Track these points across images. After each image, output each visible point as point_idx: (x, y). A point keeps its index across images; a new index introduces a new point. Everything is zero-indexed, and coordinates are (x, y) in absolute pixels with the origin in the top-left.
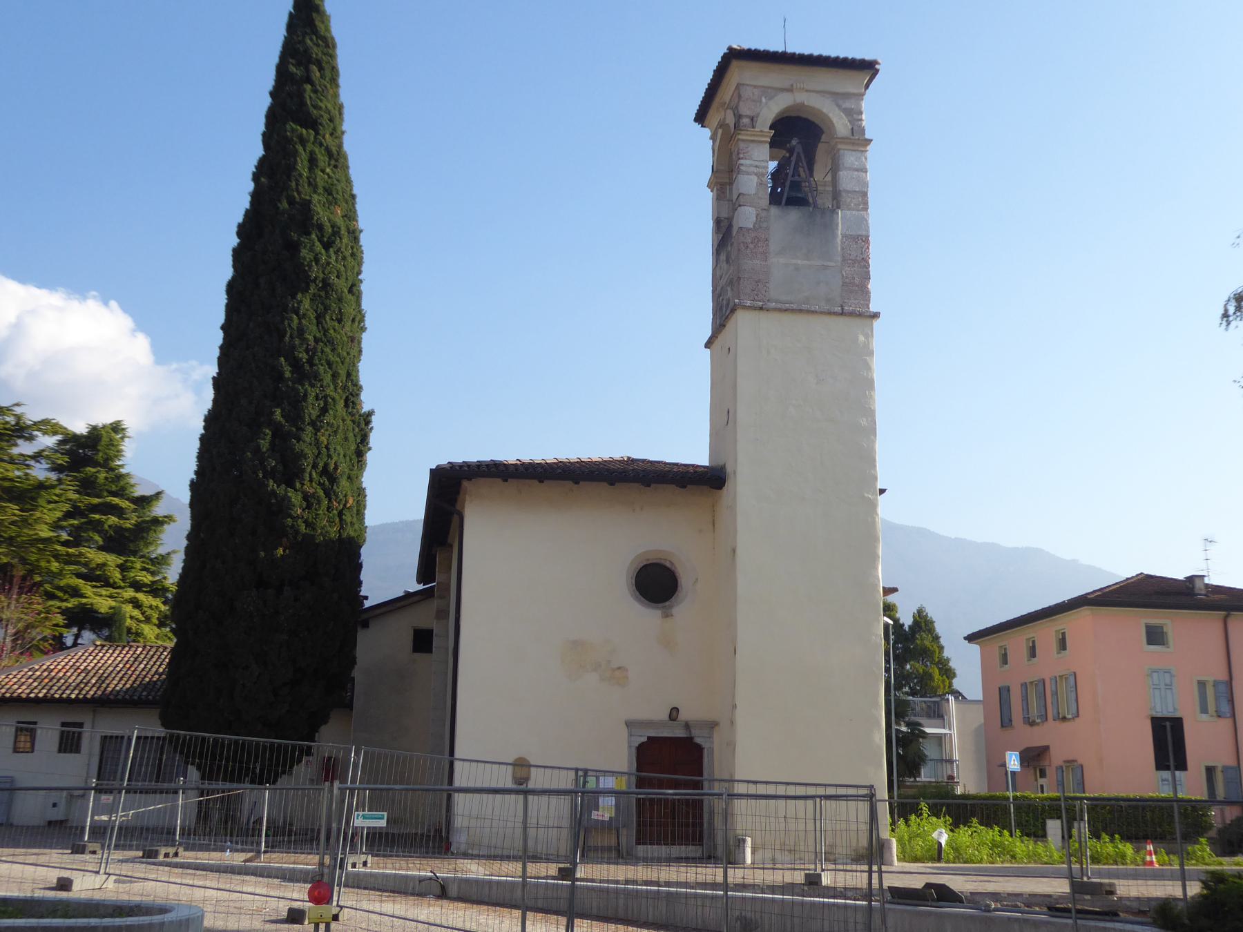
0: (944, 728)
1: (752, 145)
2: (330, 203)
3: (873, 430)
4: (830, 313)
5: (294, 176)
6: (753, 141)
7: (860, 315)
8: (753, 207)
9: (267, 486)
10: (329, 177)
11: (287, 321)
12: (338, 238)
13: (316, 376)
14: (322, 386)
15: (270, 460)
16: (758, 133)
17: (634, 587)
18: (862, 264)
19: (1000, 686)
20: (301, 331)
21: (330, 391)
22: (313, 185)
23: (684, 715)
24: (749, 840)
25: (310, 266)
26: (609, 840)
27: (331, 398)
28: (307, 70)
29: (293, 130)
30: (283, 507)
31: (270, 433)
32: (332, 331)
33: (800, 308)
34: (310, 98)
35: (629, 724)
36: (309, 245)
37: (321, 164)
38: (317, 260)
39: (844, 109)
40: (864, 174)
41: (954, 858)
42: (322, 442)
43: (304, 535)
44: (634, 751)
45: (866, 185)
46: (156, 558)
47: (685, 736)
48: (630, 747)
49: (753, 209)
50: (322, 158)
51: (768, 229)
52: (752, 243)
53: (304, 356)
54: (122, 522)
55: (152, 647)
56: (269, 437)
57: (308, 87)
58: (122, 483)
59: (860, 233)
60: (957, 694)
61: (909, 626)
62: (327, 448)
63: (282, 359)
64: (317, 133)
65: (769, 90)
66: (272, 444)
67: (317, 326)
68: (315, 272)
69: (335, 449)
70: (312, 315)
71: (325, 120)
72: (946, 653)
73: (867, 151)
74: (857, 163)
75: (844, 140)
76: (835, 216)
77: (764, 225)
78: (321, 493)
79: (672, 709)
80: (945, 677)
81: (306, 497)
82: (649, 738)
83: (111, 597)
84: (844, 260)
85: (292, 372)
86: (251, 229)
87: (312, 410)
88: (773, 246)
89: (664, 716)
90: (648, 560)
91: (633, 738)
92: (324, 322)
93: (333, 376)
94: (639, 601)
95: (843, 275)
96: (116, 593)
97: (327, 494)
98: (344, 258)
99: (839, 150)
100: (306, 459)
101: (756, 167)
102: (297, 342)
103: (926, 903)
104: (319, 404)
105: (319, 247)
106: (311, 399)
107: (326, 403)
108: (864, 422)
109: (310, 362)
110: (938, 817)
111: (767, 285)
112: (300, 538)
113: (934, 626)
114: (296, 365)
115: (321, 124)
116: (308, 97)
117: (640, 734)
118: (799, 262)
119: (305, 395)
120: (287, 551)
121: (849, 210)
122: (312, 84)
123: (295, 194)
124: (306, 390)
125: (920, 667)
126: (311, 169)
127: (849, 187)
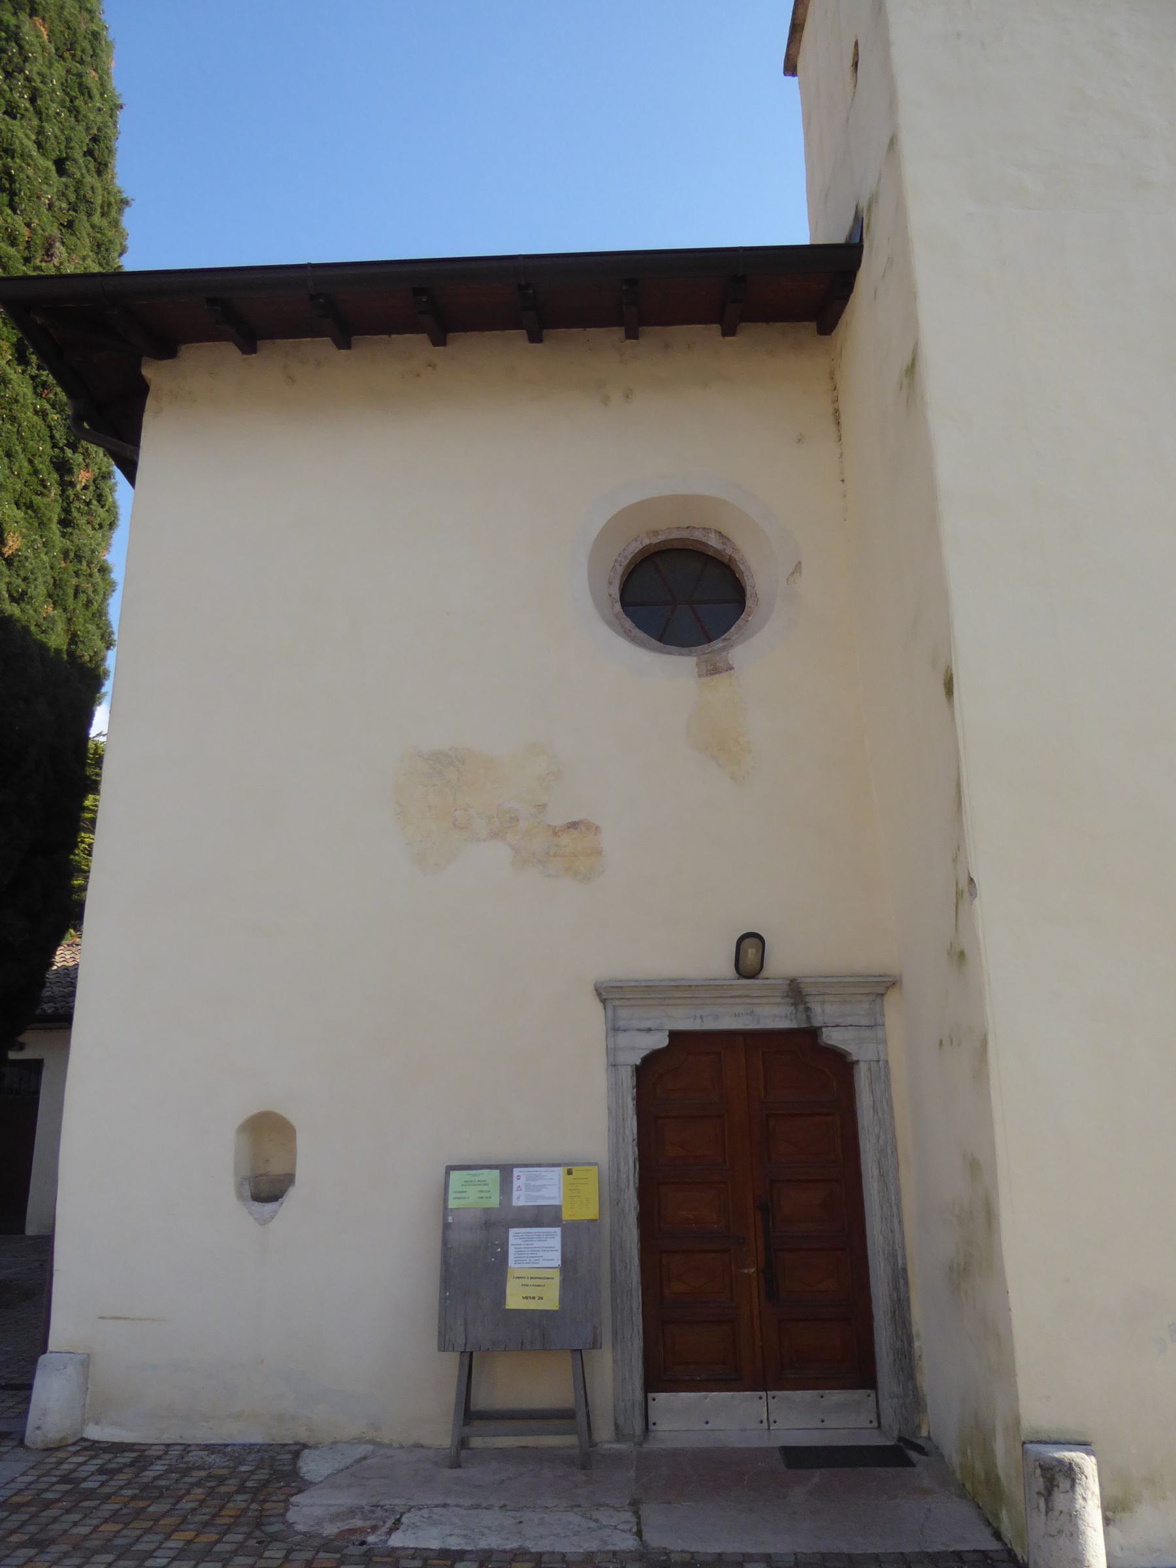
12: (13, 44)
44: (627, 1079)
47: (794, 1025)
48: (614, 1066)
89: (721, 964)
91: (623, 1039)
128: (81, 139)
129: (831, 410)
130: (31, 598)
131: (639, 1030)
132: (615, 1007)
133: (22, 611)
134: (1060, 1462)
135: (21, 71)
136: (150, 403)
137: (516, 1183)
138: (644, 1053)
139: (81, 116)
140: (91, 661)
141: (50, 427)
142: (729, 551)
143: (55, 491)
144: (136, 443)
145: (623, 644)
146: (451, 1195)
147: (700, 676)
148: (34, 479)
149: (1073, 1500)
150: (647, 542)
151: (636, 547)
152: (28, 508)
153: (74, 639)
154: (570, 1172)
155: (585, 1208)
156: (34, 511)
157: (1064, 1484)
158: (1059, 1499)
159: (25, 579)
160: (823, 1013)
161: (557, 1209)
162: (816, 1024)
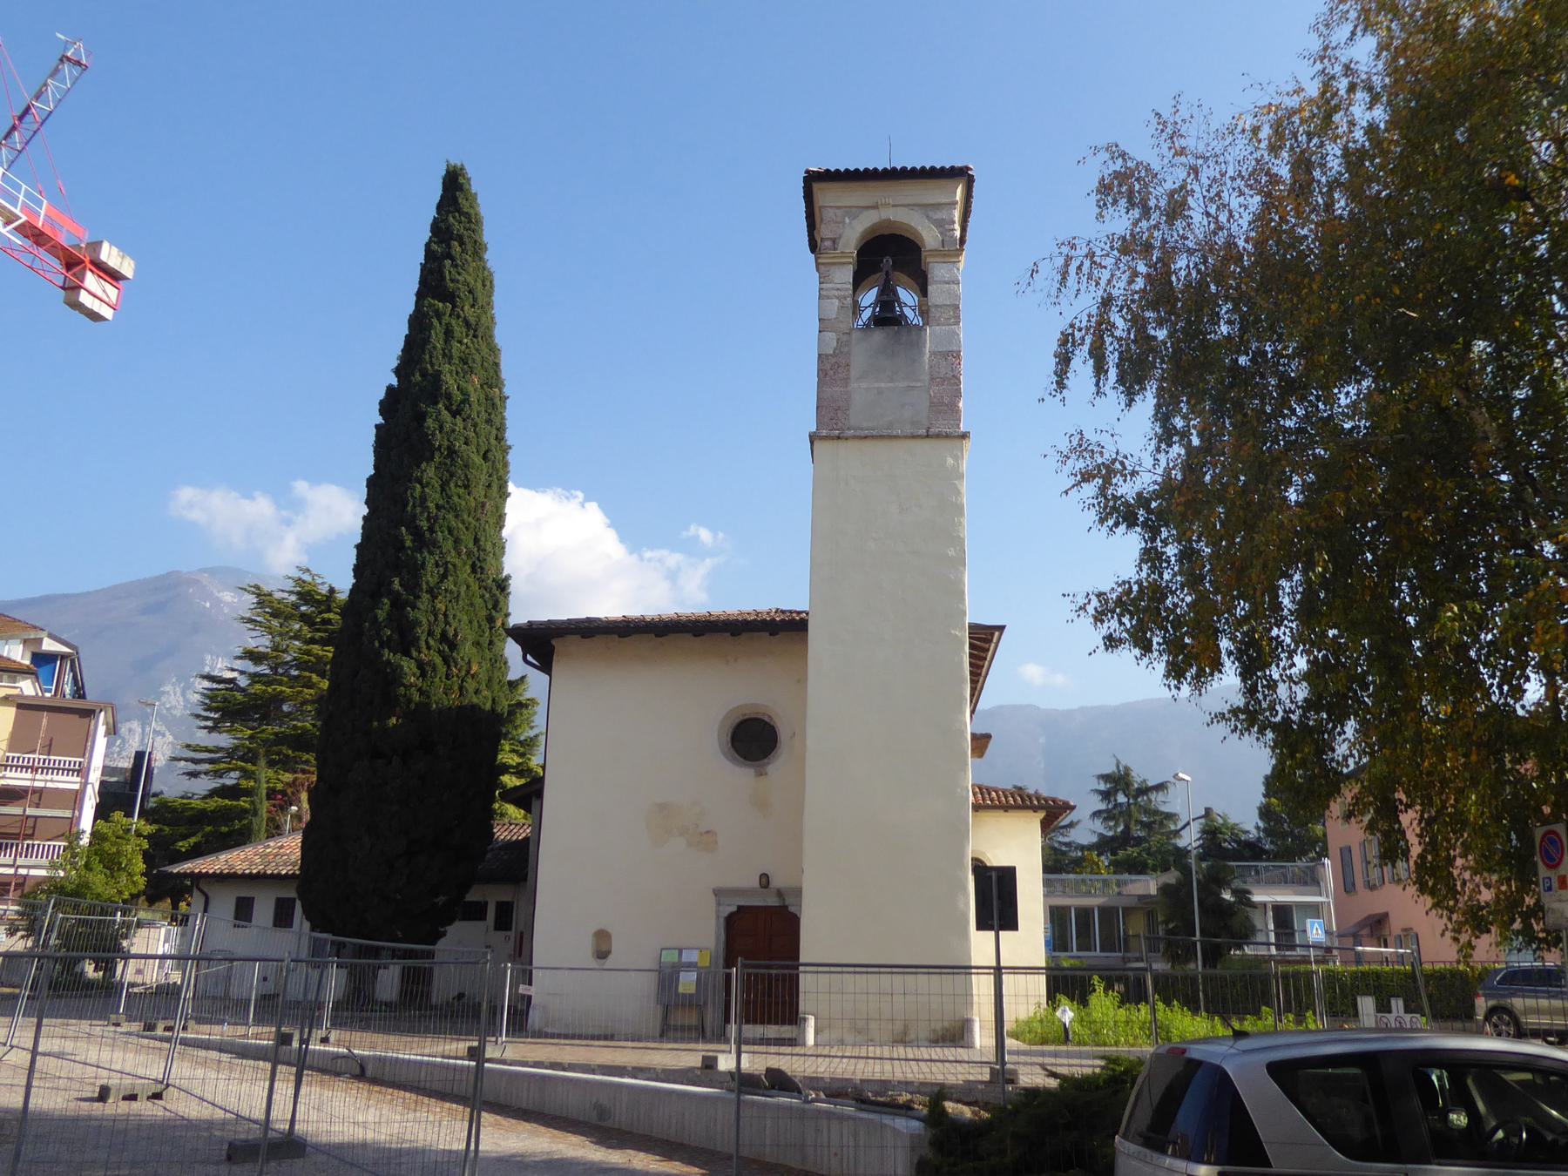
1: (833, 268)
2: (465, 373)
4: (914, 437)
7: (947, 436)
9: (383, 656)
10: (467, 347)
13: (435, 543)
18: (952, 381)
19: (1342, 846)
20: (423, 499)
21: (452, 557)
22: (448, 357)
23: (776, 882)
25: (433, 434)
26: (691, 1019)
28: (449, 246)
29: (431, 305)
30: (395, 676)
35: (718, 893)
37: (457, 335)
38: (441, 428)
40: (956, 287)
44: (722, 921)
45: (957, 297)
46: (526, 740)
48: (718, 917)
50: (458, 330)
53: (424, 525)
55: (517, 825)
56: (387, 607)
57: (448, 262)
62: (445, 615)
64: (454, 306)
66: (390, 616)
69: (454, 616)
70: (437, 484)
71: (463, 292)
75: (935, 253)
76: (923, 333)
77: (846, 349)
78: (438, 660)
81: (421, 665)
82: (740, 908)
84: (932, 379)
85: (413, 541)
86: (391, 404)
87: (430, 576)
88: (854, 373)
89: (754, 882)
91: (721, 908)
93: (455, 542)
94: (733, 760)
97: (446, 661)
98: (475, 425)
102: (418, 510)
103: (758, 1091)
105: (446, 415)
106: (430, 566)
107: (446, 570)
108: (951, 552)
109: (431, 530)
112: (412, 706)
114: (417, 534)
115: (459, 297)
118: (883, 385)
119: (423, 565)
121: (938, 325)
122: (453, 259)
126: (446, 341)
127: (939, 301)
141: (485, 601)
143: (487, 634)
151: (737, 721)
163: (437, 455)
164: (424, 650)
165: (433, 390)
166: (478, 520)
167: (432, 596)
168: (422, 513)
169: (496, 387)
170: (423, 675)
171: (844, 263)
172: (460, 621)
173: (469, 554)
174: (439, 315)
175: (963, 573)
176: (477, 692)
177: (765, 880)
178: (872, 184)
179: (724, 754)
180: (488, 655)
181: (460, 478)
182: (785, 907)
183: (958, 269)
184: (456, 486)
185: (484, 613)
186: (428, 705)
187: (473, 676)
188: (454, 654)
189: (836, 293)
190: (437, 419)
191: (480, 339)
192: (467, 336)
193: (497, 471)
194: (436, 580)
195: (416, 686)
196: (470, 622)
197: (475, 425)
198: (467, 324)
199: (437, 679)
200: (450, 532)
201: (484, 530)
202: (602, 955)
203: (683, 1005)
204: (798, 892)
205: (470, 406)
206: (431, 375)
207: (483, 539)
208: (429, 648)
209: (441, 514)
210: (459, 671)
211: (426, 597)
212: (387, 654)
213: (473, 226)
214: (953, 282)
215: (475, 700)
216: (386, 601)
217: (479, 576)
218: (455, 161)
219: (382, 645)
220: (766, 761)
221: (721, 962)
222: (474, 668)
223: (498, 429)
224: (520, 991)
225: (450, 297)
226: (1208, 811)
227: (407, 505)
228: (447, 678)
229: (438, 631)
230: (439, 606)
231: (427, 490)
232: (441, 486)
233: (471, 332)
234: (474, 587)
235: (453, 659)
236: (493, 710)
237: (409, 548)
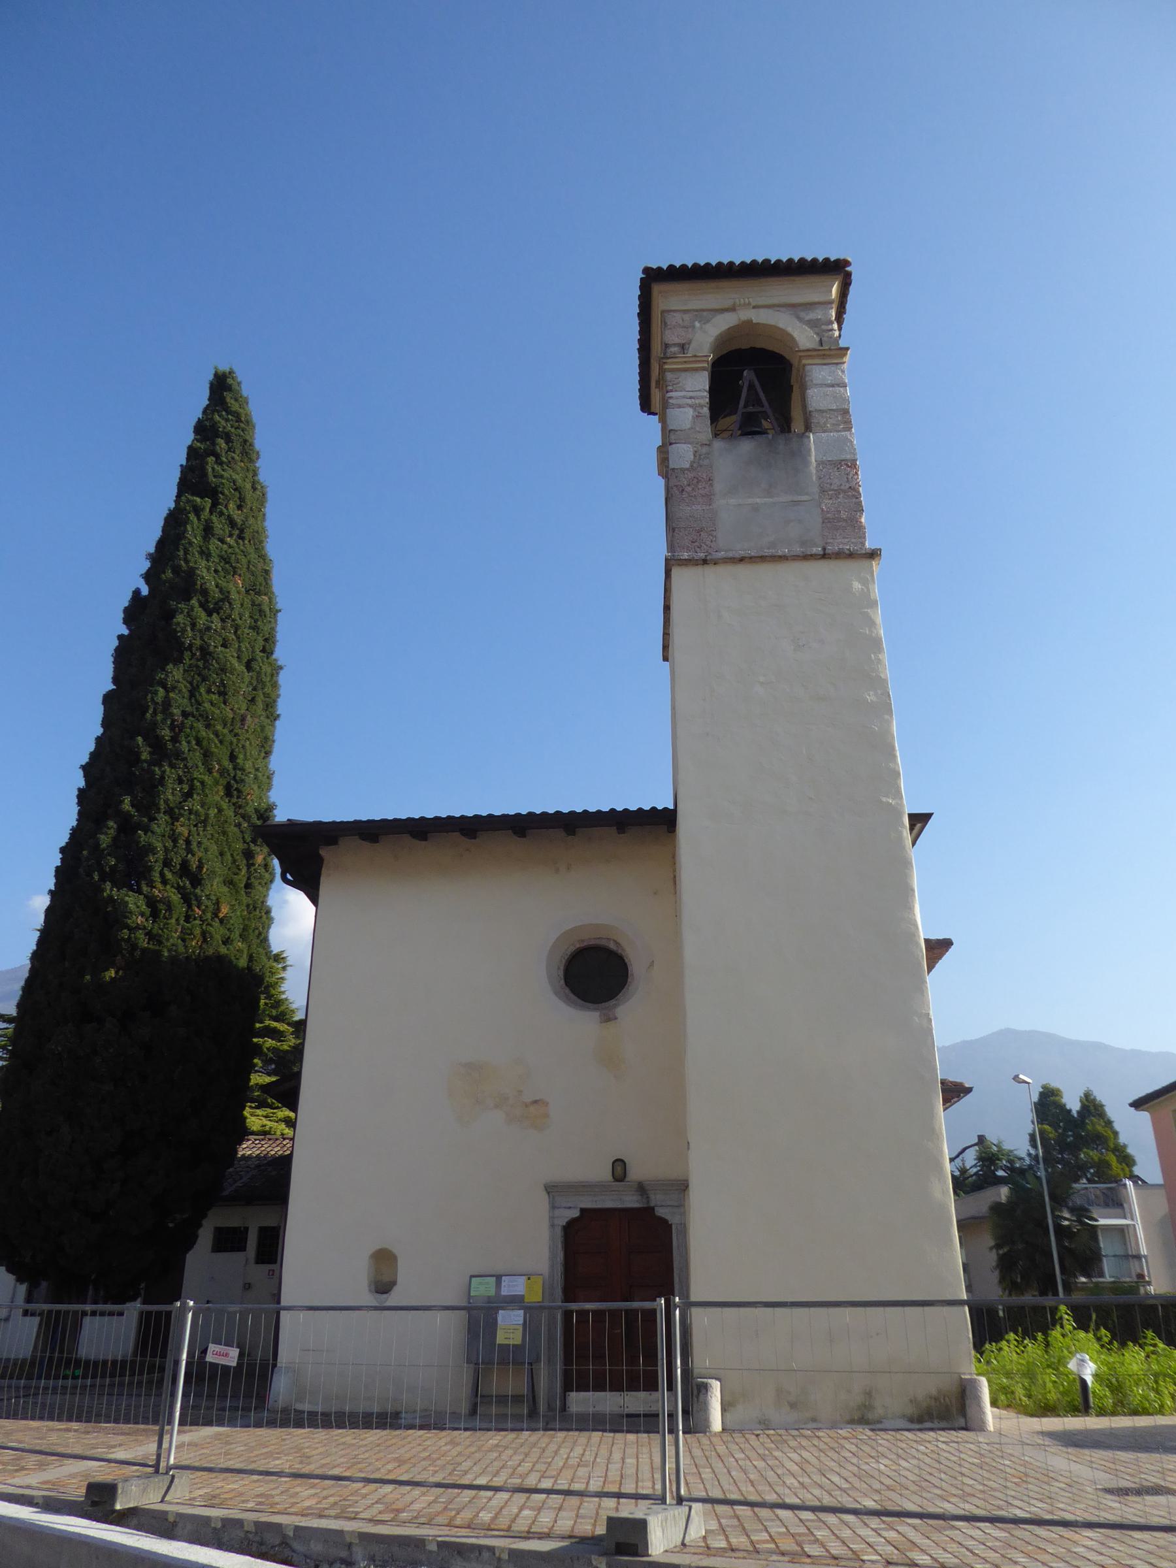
0: (1125, 1218)
1: (683, 374)
2: (226, 572)
3: (885, 708)
4: (807, 557)
5: (183, 545)
6: (686, 370)
7: (851, 555)
8: (689, 443)
9: (103, 890)
11: (150, 695)
12: (227, 603)
13: (178, 755)
14: (185, 766)
15: (109, 858)
16: (691, 359)
17: (562, 982)
20: (167, 703)
21: (199, 773)
22: (206, 554)
23: (636, 1173)
24: (716, 1386)
25: (184, 631)
26: (512, 1383)
27: (198, 781)
28: (214, 444)
29: (188, 501)
31: (115, 826)
32: (207, 705)
33: (761, 554)
34: (213, 469)
35: (552, 1190)
36: (186, 610)
38: (193, 625)
39: (808, 321)
41: (1115, 1405)
42: (180, 834)
43: (144, 950)
44: (559, 1232)
47: (641, 1206)
48: (552, 1226)
49: (689, 446)
50: (218, 525)
51: (711, 467)
52: (689, 485)
53: (166, 733)
54: (279, 1044)
58: (282, 1008)
59: (843, 457)
60: (1135, 1179)
61: (1078, 1112)
62: (188, 842)
63: (140, 739)
65: (705, 313)
67: (190, 699)
68: (189, 637)
69: (199, 843)
70: (184, 687)
72: (1122, 1139)
73: (844, 363)
74: (830, 378)
76: (805, 440)
77: (706, 462)
78: (175, 898)
79: (614, 1163)
80: (1124, 1165)
81: (152, 902)
83: (266, 1117)
84: (823, 491)
86: (136, 611)
87: (170, 793)
88: (718, 487)
89: (603, 1173)
90: (583, 941)
91: (557, 1212)
92: (197, 694)
94: (568, 1001)
95: (822, 510)
96: (273, 1113)
97: (186, 899)
98: (237, 628)
99: (804, 365)
100: (154, 854)
101: (691, 398)
104: (182, 789)
105: (202, 617)
106: (170, 783)
107: (192, 788)
108: (871, 697)
109: (175, 740)
110: (1087, 1331)
111: (714, 533)
112: (138, 953)
113: (1104, 1110)
114: (157, 745)
115: (223, 494)
116: (210, 470)
117: (569, 1205)
118: (758, 500)
119: (162, 778)
120: (121, 973)
121: (824, 432)
122: (217, 456)
123: (182, 562)
124: (164, 772)
125: (1095, 1155)
127: (823, 405)
128: (260, 643)
129: (672, 876)
130: (232, 941)
131: (565, 1208)
132: (553, 1196)
133: (228, 950)
134: (703, 1383)
135: (231, 616)
136: (324, 871)
137: (503, 1284)
138: (566, 1220)
139: (260, 631)
140: (260, 971)
141: (242, 832)
142: (620, 951)
143: (244, 871)
144: (318, 889)
145: (562, 1005)
146: (472, 1290)
147: (601, 1023)
148: (234, 866)
149: (707, 1397)
150: (578, 946)
151: (572, 949)
152: (230, 884)
153: (251, 958)
154: (529, 1279)
155: (535, 1296)
156: (234, 886)
157: (703, 1391)
158: (701, 1396)
159: (228, 930)
160: (656, 1199)
161: (522, 1297)
162: (652, 1204)
163: (187, 655)
164: (160, 886)
165: (187, 586)
166: (236, 735)
167: (171, 818)
168: (164, 721)
169: (265, 594)
170: (155, 914)
171: (696, 370)
172: (206, 850)
173: (223, 772)
174: (197, 510)
175: (889, 722)
176: (226, 941)
177: (620, 1169)
178: (725, 284)
179: (556, 993)
180: (245, 900)
181: (214, 683)
182: (649, 1211)
183: (843, 372)
184: (209, 691)
185: (239, 846)
186: (158, 953)
187: (221, 921)
188: (198, 891)
189: (689, 401)
190: (189, 615)
191: (246, 542)
192: (231, 536)
193: (264, 685)
194: (178, 799)
195: (145, 928)
196: (221, 854)
197: (237, 628)
198: (232, 523)
199: (173, 921)
200: (199, 742)
201: (243, 747)
202: (383, 1287)
203: (503, 1362)
204: (682, 1187)
205: (230, 604)
206: (184, 572)
207: (241, 756)
208: (165, 882)
209: (188, 722)
210: (204, 911)
211: (163, 818)
212: (109, 890)
213: (242, 425)
214: (838, 385)
215: (223, 950)
216: (111, 823)
217: (234, 800)
218: (224, 367)
219: (103, 879)
220: (613, 1002)
221: (559, 1292)
222: (224, 910)
223: (266, 640)
224: (210, 1358)
225: (213, 493)
226: (981, 1139)
227: (147, 711)
228: (187, 920)
229: (177, 861)
230: (180, 829)
231: (172, 695)
232: (190, 691)
233: (237, 532)
234: (229, 813)
235: (196, 896)
236: (249, 968)
237: (145, 761)
